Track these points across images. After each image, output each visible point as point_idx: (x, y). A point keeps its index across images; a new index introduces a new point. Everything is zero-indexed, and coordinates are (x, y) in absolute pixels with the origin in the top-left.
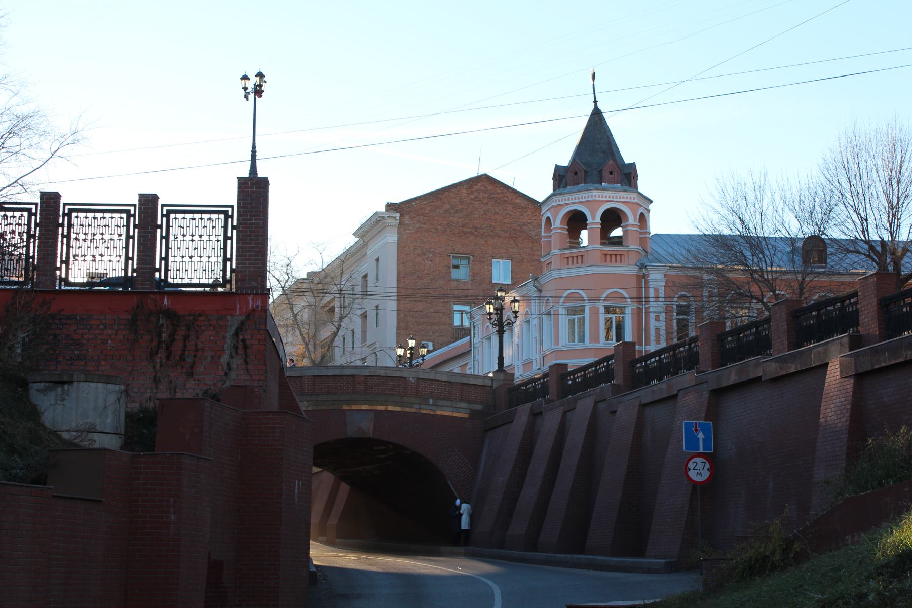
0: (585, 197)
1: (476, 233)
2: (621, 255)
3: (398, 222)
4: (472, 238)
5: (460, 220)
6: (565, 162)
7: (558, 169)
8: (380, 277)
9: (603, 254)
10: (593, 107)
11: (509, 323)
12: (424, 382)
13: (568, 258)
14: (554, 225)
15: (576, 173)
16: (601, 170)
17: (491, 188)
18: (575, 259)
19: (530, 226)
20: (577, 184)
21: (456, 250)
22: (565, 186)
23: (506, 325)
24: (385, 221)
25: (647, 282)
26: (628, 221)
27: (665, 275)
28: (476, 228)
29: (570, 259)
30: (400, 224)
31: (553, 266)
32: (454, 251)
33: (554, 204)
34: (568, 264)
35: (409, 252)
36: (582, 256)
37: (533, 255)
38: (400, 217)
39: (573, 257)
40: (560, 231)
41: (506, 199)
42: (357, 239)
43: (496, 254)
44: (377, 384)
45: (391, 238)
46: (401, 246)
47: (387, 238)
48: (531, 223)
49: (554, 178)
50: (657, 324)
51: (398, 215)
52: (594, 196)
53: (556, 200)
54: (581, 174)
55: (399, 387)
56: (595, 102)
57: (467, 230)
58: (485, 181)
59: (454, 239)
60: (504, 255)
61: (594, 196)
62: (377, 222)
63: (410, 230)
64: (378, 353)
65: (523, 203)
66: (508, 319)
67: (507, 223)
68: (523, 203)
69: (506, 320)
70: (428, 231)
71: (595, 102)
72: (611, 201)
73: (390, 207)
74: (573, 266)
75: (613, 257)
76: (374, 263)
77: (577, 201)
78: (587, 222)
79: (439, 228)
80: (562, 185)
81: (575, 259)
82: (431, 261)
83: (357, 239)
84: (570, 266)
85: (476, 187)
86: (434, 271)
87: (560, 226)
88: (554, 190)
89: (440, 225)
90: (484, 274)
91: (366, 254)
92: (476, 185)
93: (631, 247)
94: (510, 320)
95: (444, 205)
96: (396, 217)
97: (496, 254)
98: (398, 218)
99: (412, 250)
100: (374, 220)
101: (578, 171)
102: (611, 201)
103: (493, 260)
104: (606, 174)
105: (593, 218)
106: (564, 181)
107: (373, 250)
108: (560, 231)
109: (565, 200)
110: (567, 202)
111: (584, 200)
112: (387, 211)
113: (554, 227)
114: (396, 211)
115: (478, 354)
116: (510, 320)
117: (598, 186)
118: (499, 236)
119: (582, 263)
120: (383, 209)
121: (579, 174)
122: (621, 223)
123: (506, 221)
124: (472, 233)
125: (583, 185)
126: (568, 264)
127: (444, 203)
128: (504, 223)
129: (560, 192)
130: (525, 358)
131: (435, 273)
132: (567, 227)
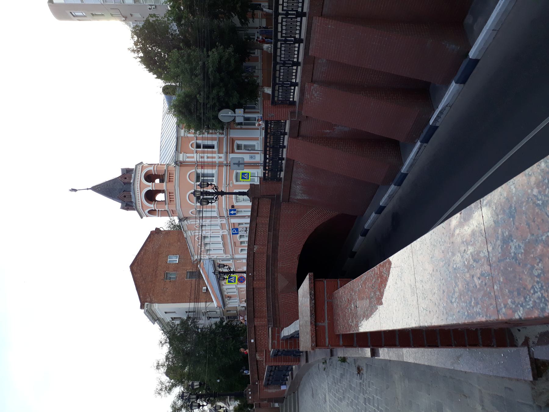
0: (138, 194)
1: (156, 270)
2: (170, 174)
3: (149, 303)
4: (158, 272)
5: (150, 277)
6: (119, 205)
7: (122, 208)
8: (174, 311)
9: (170, 202)
10: (90, 190)
11: (216, 189)
12: (257, 236)
13: (170, 201)
14: (152, 208)
15: (125, 196)
16: (123, 183)
17: (136, 264)
18: (171, 197)
19: (154, 248)
20: (131, 196)
21: (163, 278)
22: (132, 202)
23: (217, 191)
24: (148, 310)
25: (184, 162)
26: (152, 170)
27: (180, 153)
28: (154, 270)
29: (171, 199)
30: (150, 303)
31: (174, 209)
32: (163, 279)
33: (141, 208)
34: (173, 201)
35: (163, 299)
36: (169, 193)
37: (166, 247)
38: (147, 302)
39: (170, 198)
40: (155, 205)
41: (141, 258)
42: (156, 322)
43: (166, 262)
44: (258, 273)
45: (157, 307)
46: (160, 302)
47: (156, 308)
48: (153, 247)
49: (128, 210)
50: (206, 157)
51: (146, 304)
52: (137, 186)
53: (139, 207)
54: (125, 194)
55: (260, 257)
56: (88, 189)
57: (154, 274)
58: (132, 267)
59: (158, 279)
60: (166, 259)
61: (137, 186)
62: (149, 313)
63: (153, 298)
64: (207, 311)
65: (143, 251)
66: (213, 189)
67: (152, 257)
68: (143, 251)
69: (214, 190)
70: (154, 291)
71: (88, 189)
72: (141, 177)
73: (142, 307)
74: (174, 196)
75: (171, 178)
76: (167, 314)
77: (139, 195)
78: (151, 189)
79: (152, 286)
80: (131, 204)
81: (171, 197)
82: (167, 289)
83: (156, 322)
84: (174, 199)
85: (135, 270)
86: (172, 287)
87: (153, 205)
88: (134, 210)
89: (152, 285)
90: (174, 266)
91: (162, 318)
92: (134, 270)
93: (165, 169)
94: (214, 188)
95: (143, 284)
96: (147, 305)
97: (166, 262)
98: (147, 303)
99: (162, 297)
100: (148, 314)
101: (123, 195)
102: (141, 177)
103: (168, 263)
104: (126, 181)
105: (149, 186)
106: (129, 203)
107: (161, 315)
108: (155, 205)
109: (139, 201)
110: (140, 201)
111: (139, 192)
112: (144, 309)
113: (153, 208)
114: (144, 305)
115: (214, 257)
116: (214, 188)
117: (132, 185)
118: (158, 260)
119: (173, 193)
120: (143, 310)
121: (125, 194)
122: (153, 174)
123: (151, 257)
124: (156, 272)
125: (131, 193)
126: (173, 201)
127: (142, 284)
128: (152, 258)
129: (134, 205)
130: (219, 228)
131: (173, 287)
132: (154, 202)
